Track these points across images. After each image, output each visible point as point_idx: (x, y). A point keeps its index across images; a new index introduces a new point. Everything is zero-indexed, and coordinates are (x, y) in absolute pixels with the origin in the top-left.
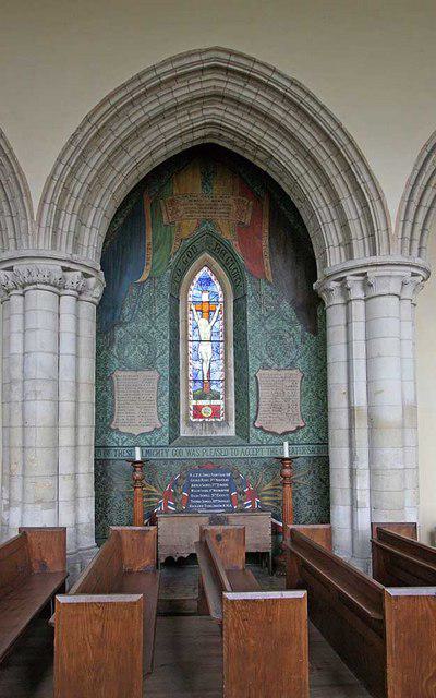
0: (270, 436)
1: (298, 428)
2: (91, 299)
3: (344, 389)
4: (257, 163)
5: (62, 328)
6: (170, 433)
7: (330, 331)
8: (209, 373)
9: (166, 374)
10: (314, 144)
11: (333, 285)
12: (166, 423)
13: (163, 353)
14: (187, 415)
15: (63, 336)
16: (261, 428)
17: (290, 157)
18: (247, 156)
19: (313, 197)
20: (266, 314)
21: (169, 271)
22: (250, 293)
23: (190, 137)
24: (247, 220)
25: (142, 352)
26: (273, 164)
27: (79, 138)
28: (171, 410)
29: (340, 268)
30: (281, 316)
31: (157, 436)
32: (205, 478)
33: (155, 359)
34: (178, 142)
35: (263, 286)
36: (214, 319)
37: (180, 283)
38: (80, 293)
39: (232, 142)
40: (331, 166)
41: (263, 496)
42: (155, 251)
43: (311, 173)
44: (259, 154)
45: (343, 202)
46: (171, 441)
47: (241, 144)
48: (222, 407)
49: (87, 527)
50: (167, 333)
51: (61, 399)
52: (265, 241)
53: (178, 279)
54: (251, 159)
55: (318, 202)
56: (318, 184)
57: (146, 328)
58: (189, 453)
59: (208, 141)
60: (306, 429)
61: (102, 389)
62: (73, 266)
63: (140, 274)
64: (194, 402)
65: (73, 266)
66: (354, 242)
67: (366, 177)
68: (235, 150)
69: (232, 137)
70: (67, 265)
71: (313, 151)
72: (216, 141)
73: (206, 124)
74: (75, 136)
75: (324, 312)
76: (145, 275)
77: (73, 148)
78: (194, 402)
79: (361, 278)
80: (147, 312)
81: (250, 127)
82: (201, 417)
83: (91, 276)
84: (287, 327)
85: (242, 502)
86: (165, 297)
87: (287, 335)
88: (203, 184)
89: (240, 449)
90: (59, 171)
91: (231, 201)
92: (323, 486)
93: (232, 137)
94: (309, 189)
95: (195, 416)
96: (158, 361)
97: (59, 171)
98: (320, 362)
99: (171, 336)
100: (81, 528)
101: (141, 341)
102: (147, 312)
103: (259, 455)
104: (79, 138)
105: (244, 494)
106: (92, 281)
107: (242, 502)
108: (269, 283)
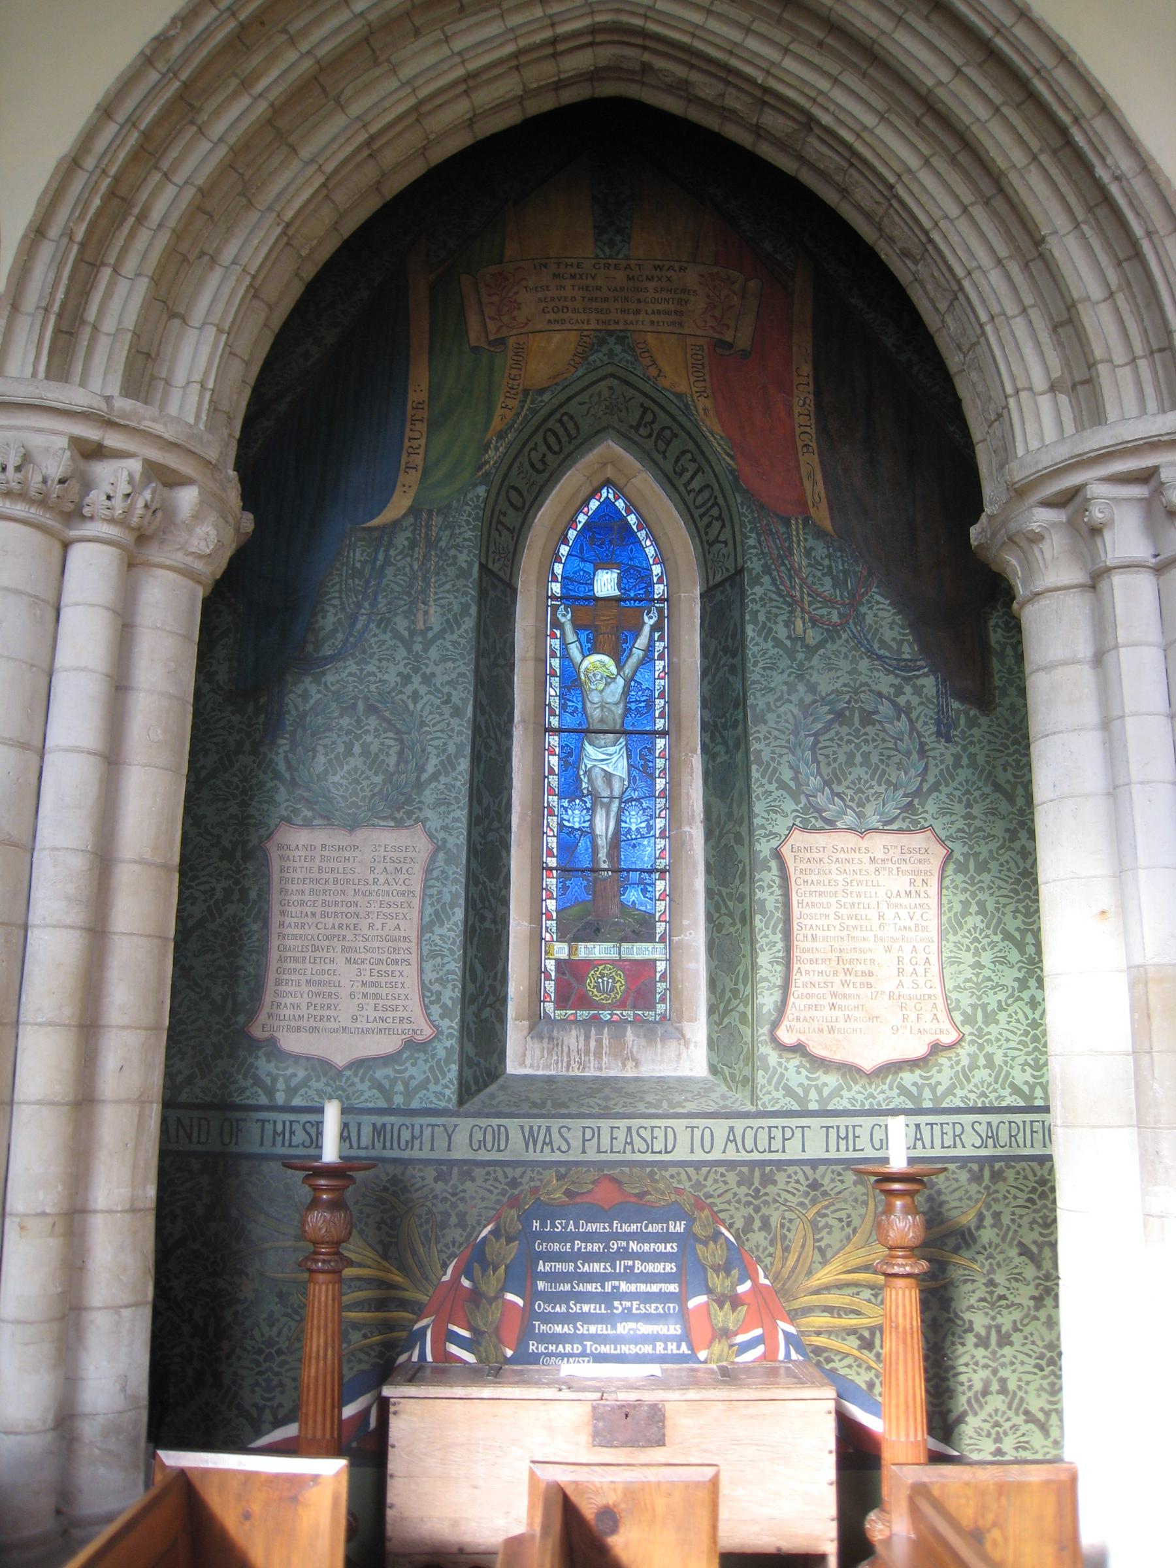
0: (832, 1080)
1: (936, 1049)
2: (179, 558)
3: (1044, 348)
4: (766, 151)
5: (64, 658)
6: (466, 1062)
7: (1039, 685)
8: (615, 843)
9: (458, 840)
10: (944, 74)
11: (1042, 517)
12: (451, 1025)
13: (448, 765)
14: (535, 996)
15: (61, 683)
16: (799, 1049)
17: (869, 119)
18: (732, 132)
19: (954, 239)
20: (813, 636)
21: (481, 491)
22: (755, 565)
23: (546, 71)
24: (743, 336)
25: (373, 761)
26: (814, 147)
27: (177, 49)
28: (469, 973)
29: (1062, 453)
30: (865, 646)
31: (417, 1071)
32: (588, 1237)
33: (419, 786)
34: (508, 87)
35: (801, 539)
36: (637, 654)
37: (518, 534)
38: (142, 538)
39: (681, 88)
40: (1005, 139)
41: (807, 1311)
42: (434, 426)
43: (939, 163)
44: (772, 120)
45: (1054, 246)
46: (466, 1092)
47: (708, 89)
48: (661, 966)
49: (112, 1429)
50: (464, 696)
51: (34, 919)
52: (802, 400)
53: (512, 518)
54: (744, 138)
55: (969, 250)
56: (967, 197)
57: (392, 678)
58: (531, 1139)
59: (608, 89)
60: (964, 1052)
61: (228, 892)
62: (113, 440)
63: (383, 501)
64: (561, 950)
65: (113, 440)
66: (1102, 369)
67: (1126, 164)
68: (696, 115)
69: (680, 71)
70: (91, 433)
71: (941, 93)
72: (633, 91)
73: (594, 30)
74: (162, 41)
75: (1014, 627)
76: (398, 506)
77: (153, 76)
78: (561, 950)
79: (1138, 491)
80: (401, 624)
81: (736, 35)
82: (584, 1002)
83: (186, 481)
84: (885, 682)
85: (726, 1334)
86: (463, 574)
87: (885, 708)
88: (596, 240)
89: (720, 1127)
90: (100, 145)
91: (691, 278)
92: (1030, 1272)
93: (680, 71)
94: (937, 214)
95: (561, 1003)
96: (429, 796)
97: (100, 145)
98: (1004, 806)
99: (479, 707)
100: (89, 1430)
101: (373, 722)
102: (401, 624)
103: (794, 1151)
104: (177, 49)
105: (736, 1302)
106: (187, 498)
107: (726, 1334)
108: (820, 534)
